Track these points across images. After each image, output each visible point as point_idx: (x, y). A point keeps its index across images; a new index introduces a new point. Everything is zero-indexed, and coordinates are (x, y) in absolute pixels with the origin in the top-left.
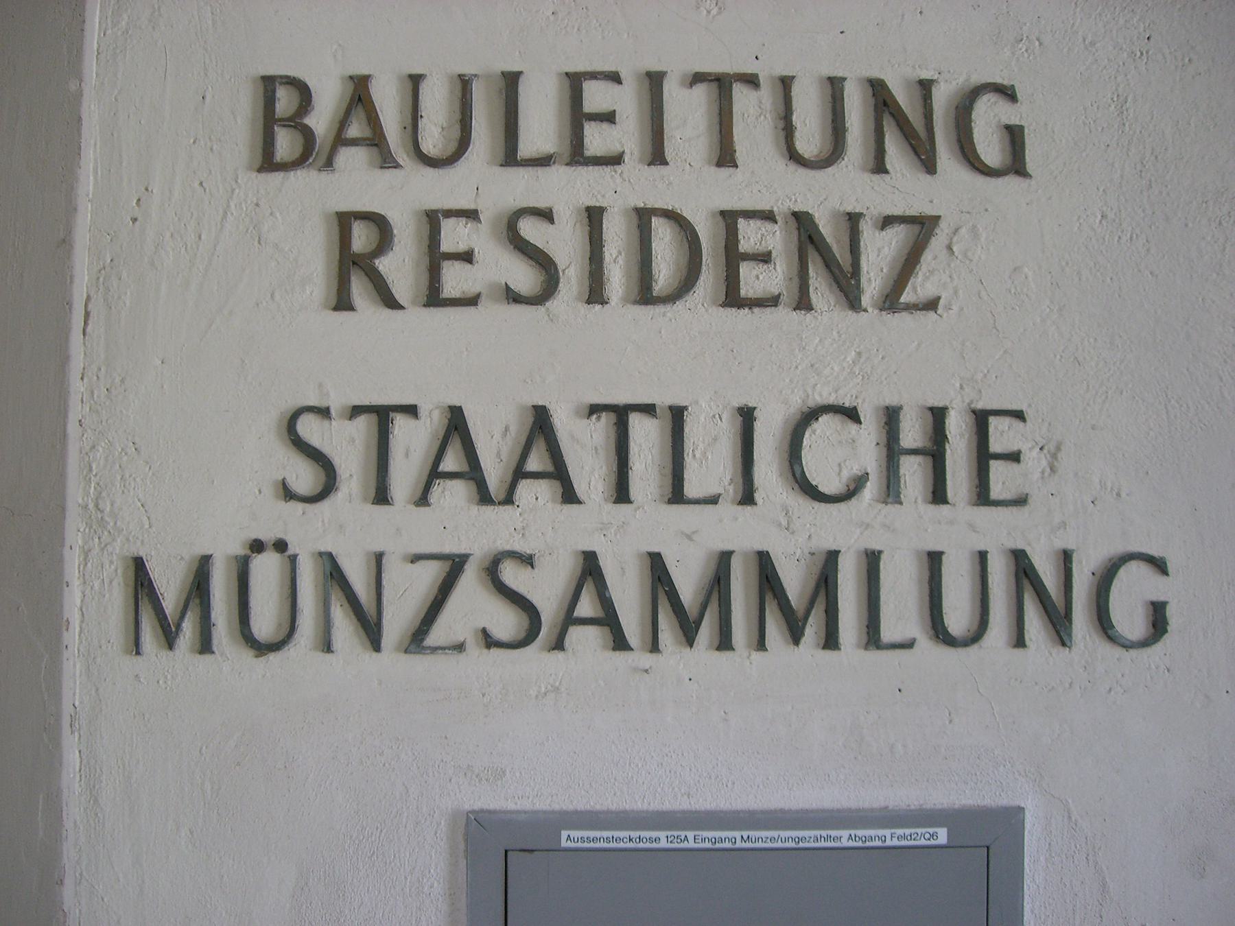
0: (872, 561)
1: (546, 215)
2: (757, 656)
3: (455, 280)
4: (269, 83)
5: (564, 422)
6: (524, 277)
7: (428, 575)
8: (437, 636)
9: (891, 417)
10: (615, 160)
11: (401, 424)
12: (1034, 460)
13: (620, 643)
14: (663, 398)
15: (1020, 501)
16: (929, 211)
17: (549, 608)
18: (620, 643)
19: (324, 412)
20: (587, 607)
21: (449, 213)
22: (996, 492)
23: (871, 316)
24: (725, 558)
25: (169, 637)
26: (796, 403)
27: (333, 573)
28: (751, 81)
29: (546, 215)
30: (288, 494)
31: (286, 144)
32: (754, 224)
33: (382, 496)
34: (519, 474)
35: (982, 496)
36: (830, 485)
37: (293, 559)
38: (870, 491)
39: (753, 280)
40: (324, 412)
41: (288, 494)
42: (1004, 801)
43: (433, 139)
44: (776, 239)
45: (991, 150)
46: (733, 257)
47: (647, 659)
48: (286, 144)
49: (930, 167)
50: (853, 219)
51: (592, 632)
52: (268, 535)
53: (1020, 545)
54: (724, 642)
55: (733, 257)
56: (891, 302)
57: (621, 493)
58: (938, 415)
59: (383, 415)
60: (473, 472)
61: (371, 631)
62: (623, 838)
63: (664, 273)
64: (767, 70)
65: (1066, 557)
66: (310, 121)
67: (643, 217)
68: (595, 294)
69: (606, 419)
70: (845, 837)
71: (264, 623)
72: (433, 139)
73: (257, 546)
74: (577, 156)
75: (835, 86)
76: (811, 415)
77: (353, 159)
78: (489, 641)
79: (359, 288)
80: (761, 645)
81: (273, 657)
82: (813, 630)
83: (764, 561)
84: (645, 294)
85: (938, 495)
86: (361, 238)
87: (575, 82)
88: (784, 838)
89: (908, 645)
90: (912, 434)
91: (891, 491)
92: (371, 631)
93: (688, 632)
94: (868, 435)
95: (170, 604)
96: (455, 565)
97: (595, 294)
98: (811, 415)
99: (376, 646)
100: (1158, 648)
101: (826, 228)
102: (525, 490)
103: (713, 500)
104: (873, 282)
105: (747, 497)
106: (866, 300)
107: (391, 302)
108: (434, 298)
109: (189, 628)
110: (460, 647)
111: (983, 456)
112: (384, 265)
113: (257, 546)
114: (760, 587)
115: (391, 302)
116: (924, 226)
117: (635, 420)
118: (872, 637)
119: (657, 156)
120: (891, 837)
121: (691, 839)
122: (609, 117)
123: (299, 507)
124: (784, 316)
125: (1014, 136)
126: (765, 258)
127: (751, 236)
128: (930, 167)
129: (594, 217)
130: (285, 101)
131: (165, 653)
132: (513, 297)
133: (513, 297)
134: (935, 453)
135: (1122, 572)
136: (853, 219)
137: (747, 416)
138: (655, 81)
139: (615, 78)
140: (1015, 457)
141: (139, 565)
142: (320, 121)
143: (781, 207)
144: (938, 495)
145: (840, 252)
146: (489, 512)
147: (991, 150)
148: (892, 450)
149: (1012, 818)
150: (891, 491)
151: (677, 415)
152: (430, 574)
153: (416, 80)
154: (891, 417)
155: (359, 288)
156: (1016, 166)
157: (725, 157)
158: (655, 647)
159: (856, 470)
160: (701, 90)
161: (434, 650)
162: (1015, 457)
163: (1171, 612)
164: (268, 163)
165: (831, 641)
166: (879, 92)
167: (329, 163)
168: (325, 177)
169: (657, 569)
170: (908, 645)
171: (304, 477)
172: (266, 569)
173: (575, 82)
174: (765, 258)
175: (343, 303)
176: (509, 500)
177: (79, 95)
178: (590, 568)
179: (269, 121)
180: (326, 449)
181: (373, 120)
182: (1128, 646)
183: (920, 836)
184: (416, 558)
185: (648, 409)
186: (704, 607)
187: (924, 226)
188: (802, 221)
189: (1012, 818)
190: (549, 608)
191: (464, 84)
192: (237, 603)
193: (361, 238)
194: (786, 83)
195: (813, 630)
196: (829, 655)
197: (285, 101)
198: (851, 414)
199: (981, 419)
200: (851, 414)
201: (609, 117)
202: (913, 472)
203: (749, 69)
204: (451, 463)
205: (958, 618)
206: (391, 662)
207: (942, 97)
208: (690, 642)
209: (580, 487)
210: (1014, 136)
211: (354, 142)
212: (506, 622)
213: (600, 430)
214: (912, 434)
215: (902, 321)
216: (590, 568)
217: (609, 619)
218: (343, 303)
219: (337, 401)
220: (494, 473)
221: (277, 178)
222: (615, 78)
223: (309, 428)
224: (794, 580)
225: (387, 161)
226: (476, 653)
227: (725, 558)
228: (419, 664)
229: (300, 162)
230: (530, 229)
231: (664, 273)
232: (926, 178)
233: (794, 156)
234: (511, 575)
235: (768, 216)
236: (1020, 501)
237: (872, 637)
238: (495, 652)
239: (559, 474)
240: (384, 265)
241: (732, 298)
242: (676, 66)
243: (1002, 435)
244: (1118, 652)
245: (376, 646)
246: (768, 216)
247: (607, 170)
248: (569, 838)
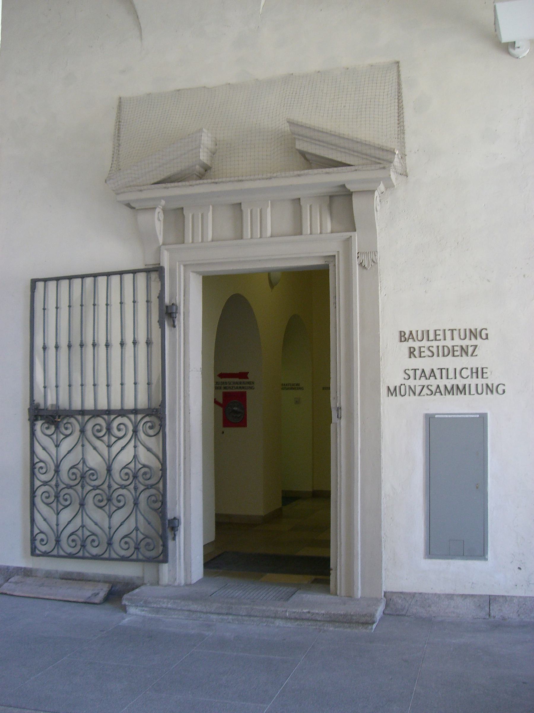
0: (470, 385)
1: (433, 347)
2: (457, 396)
3: (423, 354)
4: (401, 332)
5: (435, 370)
6: (430, 354)
7: (421, 388)
8: (421, 394)
9: (472, 369)
10: (440, 340)
11: (417, 371)
12: (489, 373)
13: (442, 395)
14: (446, 367)
15: (487, 378)
16: (476, 344)
17: (434, 391)
18: (442, 395)
19: (409, 370)
20: (438, 391)
21: (422, 347)
22: (484, 377)
23: (469, 357)
24: (453, 385)
25: (392, 395)
26: (461, 367)
27: (410, 388)
28: (456, 330)
29: (433, 347)
30: (405, 379)
31: (403, 339)
32: (456, 347)
33: (415, 379)
34: (430, 376)
35: (483, 377)
36: (465, 377)
37: (406, 386)
38: (469, 377)
39: (456, 354)
40: (409, 370)
41: (405, 379)
42: (486, 412)
43: (420, 338)
44: (458, 348)
45: (484, 336)
46: (454, 351)
47: (445, 396)
48: (403, 339)
49: (476, 339)
50: (468, 346)
51: (439, 393)
52: (403, 383)
53: (487, 383)
54: (453, 394)
55: (454, 351)
56: (472, 355)
57: (442, 378)
58: (477, 368)
59: (415, 370)
60: (425, 376)
61: (414, 394)
62: (442, 416)
63: (446, 353)
64: (457, 328)
65: (493, 384)
66: (405, 336)
67: (443, 347)
68: (438, 356)
69: (440, 370)
70: (467, 416)
71: (403, 393)
72: (420, 338)
73: (402, 385)
74: (436, 340)
75: (465, 330)
76: (463, 369)
77: (410, 340)
78: (427, 395)
79: (412, 355)
80: (457, 394)
81: (404, 397)
82: (463, 393)
83: (457, 385)
84: (444, 356)
85: (477, 377)
86: (412, 350)
87: (435, 331)
88: (460, 416)
89: (474, 394)
90: (474, 371)
91: (472, 377)
92: (414, 394)
93: (449, 393)
94: (469, 371)
95: (392, 391)
96: (424, 386)
97: (438, 356)
98: (463, 369)
99: (415, 395)
100: (504, 394)
101: (464, 347)
102: (431, 378)
103: (452, 379)
104: (470, 353)
105: (456, 378)
106: (469, 355)
107: (415, 357)
108: (420, 357)
109: (394, 394)
110: (424, 395)
111: (483, 373)
112: (415, 353)
113: (402, 385)
114: (33, 364)
115: (415, 357)
116: (476, 346)
117: (443, 370)
118: (470, 393)
119: (445, 339)
120: (472, 416)
121: (450, 416)
122: (439, 335)
123: (406, 380)
124: (459, 357)
125: (487, 335)
126: (457, 351)
127: (456, 348)
128: (476, 339)
129: (438, 347)
130: (403, 334)
131: (392, 397)
132: (429, 356)
133: (429, 356)
134: (477, 372)
135: (499, 386)
136: (468, 346)
137: (455, 369)
138: (445, 330)
139: (440, 330)
140: (486, 373)
141: (388, 387)
142: (407, 336)
143: (459, 345)
144: (477, 377)
145: (466, 350)
146: (427, 380)
147: (484, 336)
148: (472, 373)
149: (486, 414)
150: (472, 377)
151: (448, 369)
152: (421, 387)
153: (417, 331)
154: (472, 369)
155: (412, 355)
156: (487, 338)
157: (453, 339)
158: (445, 395)
159: (467, 375)
160: (450, 331)
161: (421, 396)
162: (486, 373)
163: (505, 390)
164: (401, 341)
165: (465, 394)
166: (471, 331)
167: (408, 341)
168: (408, 343)
169: (446, 387)
170: (474, 394)
171: (407, 377)
172: (403, 387)
173: (435, 331)
174: (457, 351)
175: (410, 357)
176: (429, 379)
177: (379, 334)
178: (438, 386)
179: (401, 337)
180: (409, 374)
181: (413, 336)
182: (500, 394)
183: (475, 416)
184: (419, 386)
185: (444, 369)
186: (463, 389)
187: (476, 346)
188: (462, 347)
189: (486, 414)
190: (434, 391)
191: (423, 331)
192: (201, 392)
193: (412, 350)
194: (460, 330)
195: (463, 393)
196: (465, 396)
197: (403, 334)
198: (467, 369)
199: (483, 369)
200: (467, 369)
201: (439, 335)
202: (474, 375)
203: (455, 328)
204: (423, 375)
205: (480, 392)
206: (417, 397)
207: (478, 330)
208: (449, 394)
209: (437, 377)
210: (487, 335)
211: (411, 339)
212: (429, 392)
213: (439, 371)
214: (474, 371)
215: (473, 358)
216: (438, 386)
217: (440, 392)
218: (410, 357)
219: (410, 368)
220: (428, 376)
221: (402, 343)
222: (440, 330)
223: (407, 371)
224: (461, 388)
225: (414, 341)
226: (426, 396)
227: (453, 385)
228: (420, 397)
229: (405, 341)
230: (431, 348)
231: (446, 353)
232: (476, 341)
233: (461, 339)
234: (429, 387)
235: (458, 346)
236: (487, 378)
237: (470, 393)
238: (428, 396)
239: (435, 376)
240: (415, 353)
241: (454, 356)
242: (447, 328)
243: (485, 370)
244: (499, 395)
245: (415, 395)
246: (458, 346)
247: (439, 341)
248: (436, 416)
